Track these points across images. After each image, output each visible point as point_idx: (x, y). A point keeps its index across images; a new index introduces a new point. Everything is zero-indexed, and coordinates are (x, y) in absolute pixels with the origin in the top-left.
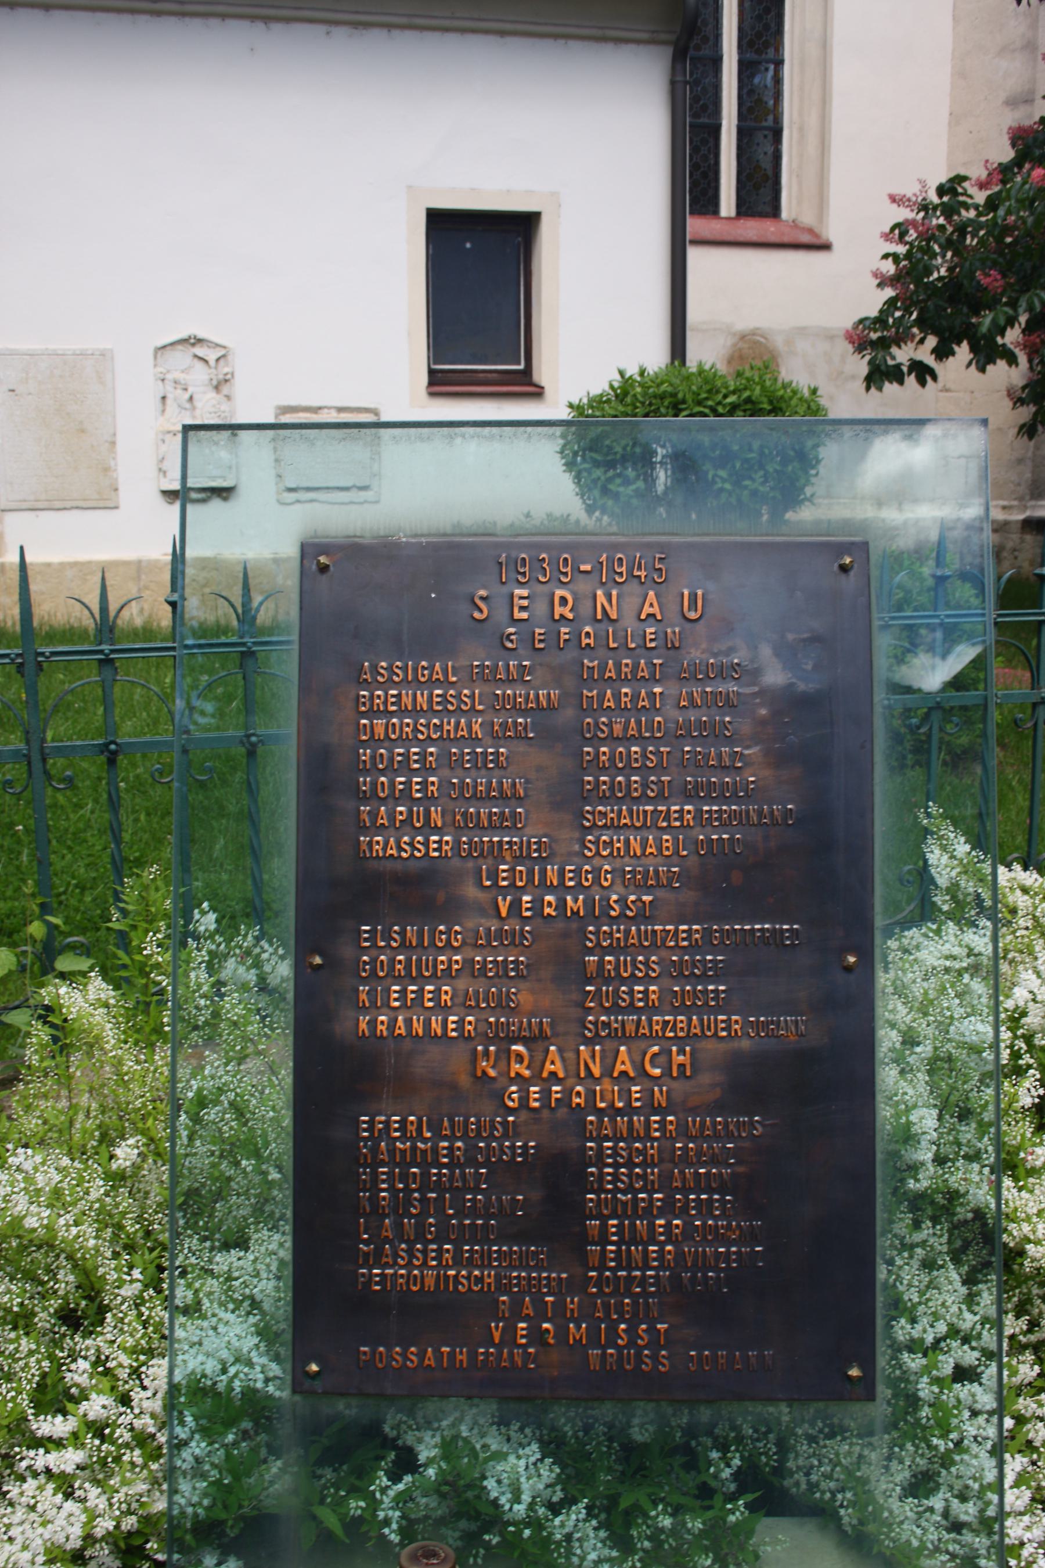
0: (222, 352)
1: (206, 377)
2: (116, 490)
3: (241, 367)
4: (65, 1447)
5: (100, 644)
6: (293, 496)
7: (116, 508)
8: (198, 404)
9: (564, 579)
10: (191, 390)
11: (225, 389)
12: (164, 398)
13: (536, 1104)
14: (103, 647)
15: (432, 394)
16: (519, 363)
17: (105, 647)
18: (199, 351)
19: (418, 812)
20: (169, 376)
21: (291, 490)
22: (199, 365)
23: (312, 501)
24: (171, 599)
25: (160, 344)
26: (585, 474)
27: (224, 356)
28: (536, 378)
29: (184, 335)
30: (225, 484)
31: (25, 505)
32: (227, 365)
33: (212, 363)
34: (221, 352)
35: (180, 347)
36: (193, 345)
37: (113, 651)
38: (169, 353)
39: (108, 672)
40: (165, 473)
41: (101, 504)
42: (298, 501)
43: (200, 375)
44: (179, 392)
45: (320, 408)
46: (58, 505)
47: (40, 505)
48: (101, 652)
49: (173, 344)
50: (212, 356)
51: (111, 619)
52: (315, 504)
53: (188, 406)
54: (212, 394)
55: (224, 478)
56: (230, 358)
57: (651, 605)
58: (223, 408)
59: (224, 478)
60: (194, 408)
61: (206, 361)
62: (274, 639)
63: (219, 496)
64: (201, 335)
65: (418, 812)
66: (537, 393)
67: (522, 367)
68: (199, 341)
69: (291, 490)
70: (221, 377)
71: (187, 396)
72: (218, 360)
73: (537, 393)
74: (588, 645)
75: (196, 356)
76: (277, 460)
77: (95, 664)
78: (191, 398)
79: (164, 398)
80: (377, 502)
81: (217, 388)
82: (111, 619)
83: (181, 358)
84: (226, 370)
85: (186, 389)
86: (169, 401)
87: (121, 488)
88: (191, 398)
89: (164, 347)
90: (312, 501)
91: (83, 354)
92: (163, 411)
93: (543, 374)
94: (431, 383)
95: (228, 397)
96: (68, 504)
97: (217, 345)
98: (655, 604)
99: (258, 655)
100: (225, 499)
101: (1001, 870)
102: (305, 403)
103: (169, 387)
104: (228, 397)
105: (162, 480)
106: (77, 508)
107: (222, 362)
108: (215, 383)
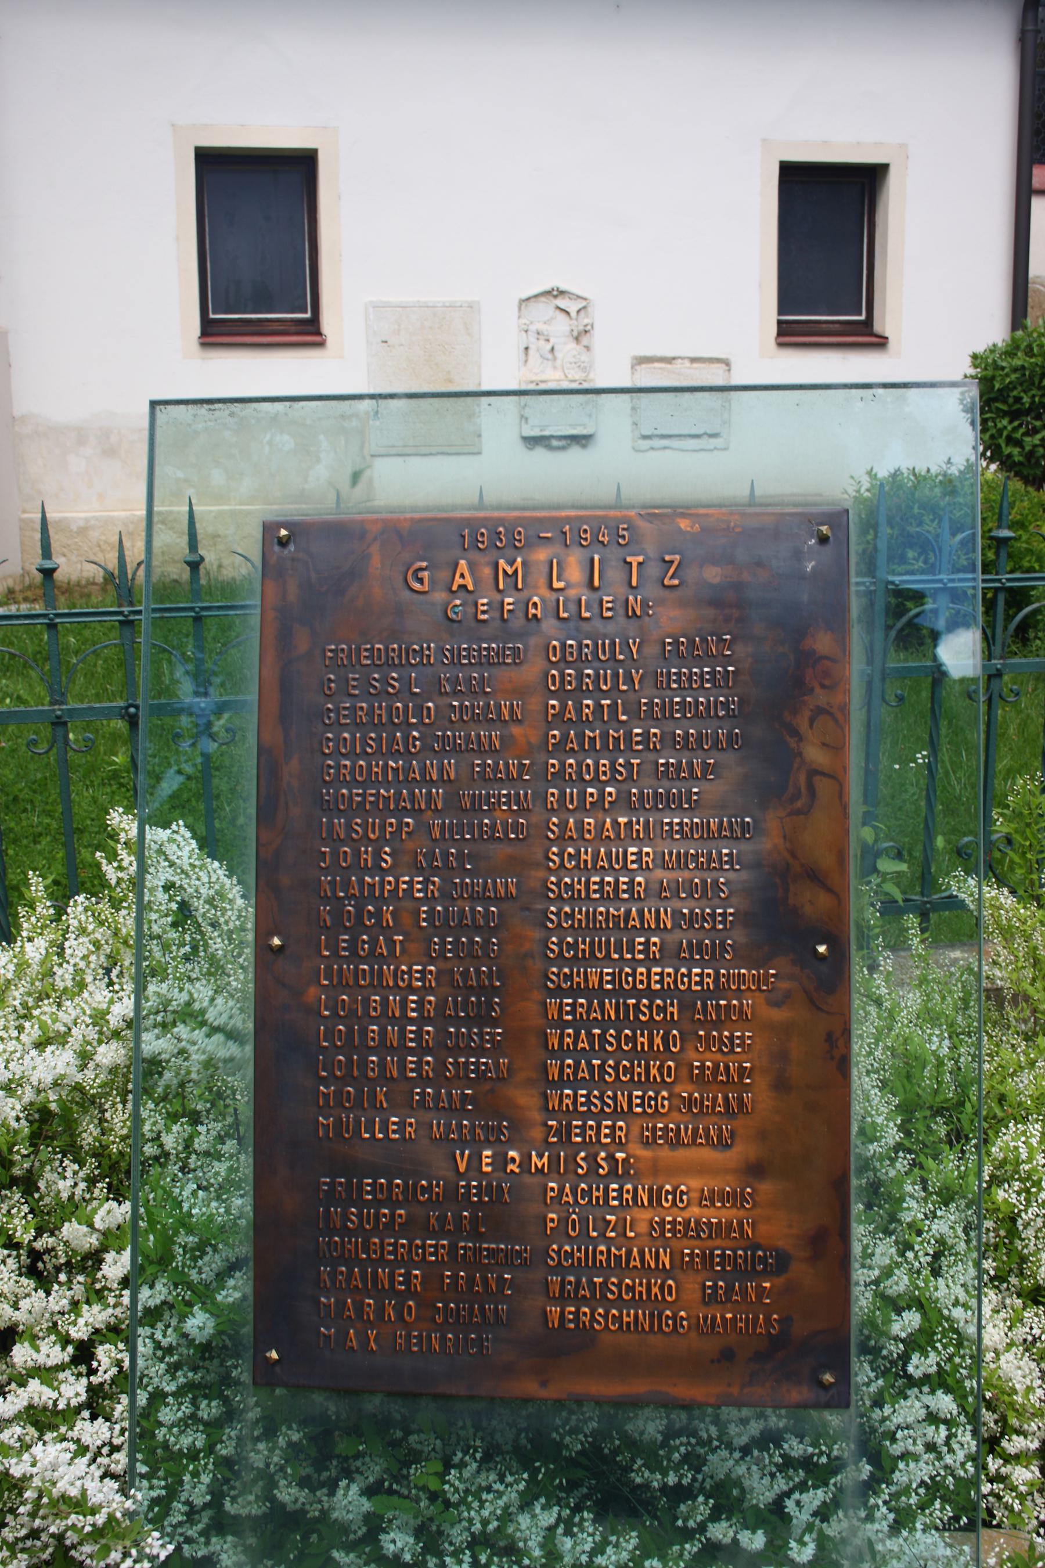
0: (584, 303)
1: (568, 328)
2: (480, 436)
3: (600, 318)
4: (812, 1515)
5: (120, 606)
6: (647, 443)
7: (480, 453)
8: (559, 354)
9: (584, 543)
10: (552, 340)
11: (585, 340)
12: (527, 349)
13: (489, 1169)
14: (941, 577)
15: (781, 345)
16: (860, 314)
17: (126, 609)
18: (562, 303)
19: (572, 794)
20: (533, 328)
21: (645, 437)
22: (561, 316)
23: (665, 448)
24: (189, 559)
25: (524, 296)
26: (990, 424)
27: (584, 308)
28: (877, 328)
29: (547, 287)
30: (585, 432)
31: (393, 451)
32: (587, 316)
33: (573, 314)
34: (581, 304)
35: (543, 299)
36: (555, 297)
37: (952, 581)
38: (532, 304)
39: (127, 631)
40: (527, 419)
41: (466, 450)
42: (652, 449)
43: (561, 326)
44: (542, 342)
45: (674, 358)
46: (424, 450)
47: (408, 451)
48: (121, 613)
49: (536, 296)
50: (573, 307)
51: (130, 577)
52: (667, 451)
53: (550, 356)
54: (572, 345)
55: (584, 426)
56: (589, 309)
57: (462, 576)
58: (583, 358)
59: (584, 426)
60: (555, 359)
61: (568, 313)
62: (248, 602)
63: (578, 443)
64: (563, 287)
65: (572, 794)
66: (880, 343)
67: (863, 317)
68: (562, 293)
69: (645, 437)
70: (581, 328)
71: (549, 347)
72: (578, 311)
73: (880, 343)
74: (535, 616)
75: (558, 308)
76: (634, 409)
77: (191, 620)
78: (553, 349)
79: (527, 349)
80: (726, 449)
81: (577, 339)
82: (130, 577)
83: (544, 309)
84: (586, 321)
85: (548, 340)
86: (531, 352)
87: (484, 434)
88: (553, 349)
89: (528, 299)
90: (665, 448)
91: (452, 306)
92: (526, 361)
93: (886, 323)
94: (780, 334)
95: (587, 348)
96: (434, 450)
97: (579, 297)
98: (467, 574)
99: (60, 627)
100: (584, 446)
101: (986, 889)
102: (660, 353)
103: (532, 338)
104: (587, 348)
105: (524, 426)
106: (443, 453)
107: (582, 313)
108: (575, 333)
